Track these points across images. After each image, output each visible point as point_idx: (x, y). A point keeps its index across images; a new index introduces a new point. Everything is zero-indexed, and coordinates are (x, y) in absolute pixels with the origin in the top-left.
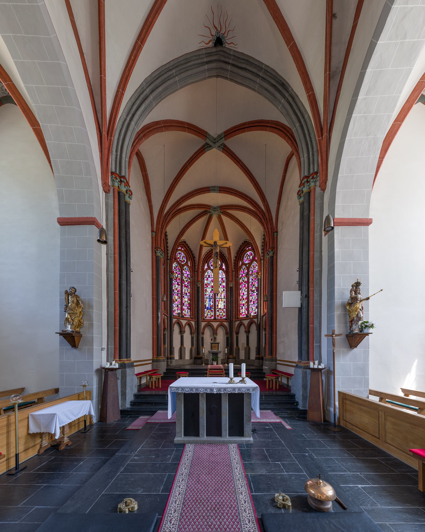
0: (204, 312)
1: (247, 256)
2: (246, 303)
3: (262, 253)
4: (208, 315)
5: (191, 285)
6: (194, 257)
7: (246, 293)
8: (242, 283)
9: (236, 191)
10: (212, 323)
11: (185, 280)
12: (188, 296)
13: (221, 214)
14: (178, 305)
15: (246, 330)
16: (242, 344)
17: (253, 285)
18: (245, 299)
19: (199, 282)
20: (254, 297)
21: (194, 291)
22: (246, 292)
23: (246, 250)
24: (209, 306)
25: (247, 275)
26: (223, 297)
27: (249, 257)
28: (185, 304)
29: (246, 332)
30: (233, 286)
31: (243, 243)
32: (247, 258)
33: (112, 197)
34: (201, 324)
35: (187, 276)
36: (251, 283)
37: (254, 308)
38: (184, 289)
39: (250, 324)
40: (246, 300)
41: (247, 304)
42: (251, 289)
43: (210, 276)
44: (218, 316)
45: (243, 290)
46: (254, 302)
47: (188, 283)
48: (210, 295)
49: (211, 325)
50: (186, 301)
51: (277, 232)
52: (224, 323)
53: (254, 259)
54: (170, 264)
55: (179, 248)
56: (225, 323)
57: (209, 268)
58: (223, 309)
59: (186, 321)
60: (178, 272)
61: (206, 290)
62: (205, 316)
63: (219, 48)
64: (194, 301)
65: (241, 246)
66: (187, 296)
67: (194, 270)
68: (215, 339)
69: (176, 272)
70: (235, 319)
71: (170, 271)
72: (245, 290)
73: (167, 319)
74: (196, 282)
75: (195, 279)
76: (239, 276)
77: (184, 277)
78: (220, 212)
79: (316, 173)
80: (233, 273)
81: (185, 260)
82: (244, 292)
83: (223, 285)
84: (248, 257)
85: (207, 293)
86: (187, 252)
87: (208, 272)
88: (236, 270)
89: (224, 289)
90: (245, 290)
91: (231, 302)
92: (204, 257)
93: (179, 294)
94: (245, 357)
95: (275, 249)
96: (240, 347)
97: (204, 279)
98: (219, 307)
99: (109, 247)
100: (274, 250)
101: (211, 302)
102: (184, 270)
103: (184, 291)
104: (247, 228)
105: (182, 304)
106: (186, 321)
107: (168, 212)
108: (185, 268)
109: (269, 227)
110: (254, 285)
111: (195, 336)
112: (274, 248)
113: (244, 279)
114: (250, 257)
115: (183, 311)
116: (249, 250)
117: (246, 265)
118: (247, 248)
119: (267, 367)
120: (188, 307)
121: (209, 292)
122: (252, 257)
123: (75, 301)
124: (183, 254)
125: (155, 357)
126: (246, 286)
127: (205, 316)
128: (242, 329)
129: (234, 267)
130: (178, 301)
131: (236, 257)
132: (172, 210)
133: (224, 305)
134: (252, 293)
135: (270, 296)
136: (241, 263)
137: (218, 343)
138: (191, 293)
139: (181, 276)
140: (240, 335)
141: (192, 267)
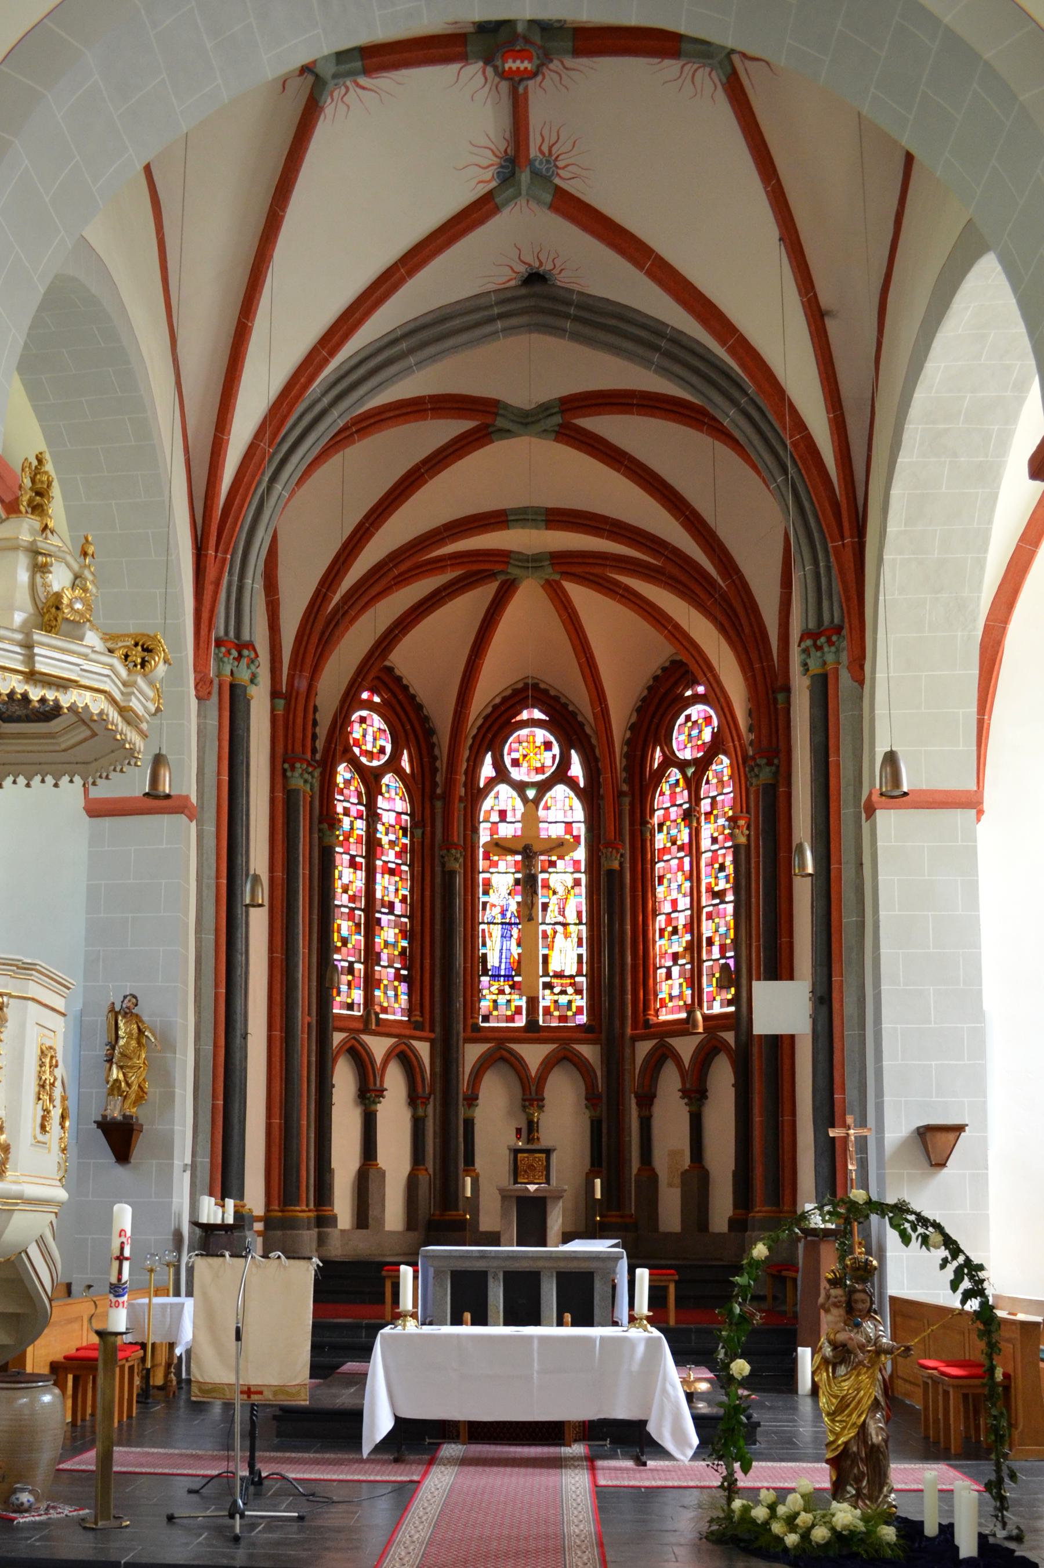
0: (475, 992)
1: (690, 724)
2: (686, 949)
4: (496, 1007)
6: (430, 732)
7: (688, 899)
8: (665, 850)
9: (633, 460)
10: (516, 1047)
11: (385, 840)
13: (557, 577)
15: (688, 1086)
16: (673, 1154)
17: (716, 866)
18: (680, 932)
19: (453, 851)
21: (428, 893)
24: (501, 962)
25: (689, 816)
26: (571, 917)
27: (695, 733)
28: (384, 956)
29: (685, 1093)
30: (621, 864)
32: (689, 735)
33: (216, 708)
34: (461, 1051)
36: (710, 854)
40: (688, 937)
41: (692, 958)
42: (709, 889)
43: (509, 814)
44: (547, 1011)
45: (674, 886)
46: (723, 948)
47: (398, 855)
48: (508, 905)
49: (513, 1059)
50: (391, 940)
52: (577, 1047)
56: (588, 1051)
58: (572, 977)
59: (389, 1042)
60: (353, 812)
61: (487, 884)
62: (483, 1011)
63: (537, 289)
64: (427, 939)
65: (656, 678)
67: (427, 790)
68: (531, 1129)
69: (345, 808)
70: (634, 1027)
72: (680, 886)
74: (441, 849)
76: (652, 815)
77: (380, 827)
79: (838, 630)
80: (620, 804)
81: (388, 748)
82: (674, 895)
84: (691, 729)
85: (493, 898)
86: (398, 708)
87: (497, 797)
88: (637, 787)
89: (577, 876)
90: (680, 886)
91: (616, 942)
92: (479, 728)
93: (360, 909)
94: (683, 1222)
98: (554, 966)
99: (205, 856)
100: (776, 761)
101: (514, 942)
102: (382, 794)
103: (379, 895)
104: (677, 627)
105: (371, 956)
106: (389, 1042)
108: (388, 786)
110: (722, 868)
111: (431, 1112)
112: (776, 753)
113: (674, 832)
114: (700, 732)
115: (377, 993)
116: (697, 699)
117: (682, 765)
120: (398, 970)
121: (504, 891)
123: (135, 1031)
124: (377, 721)
126: (687, 867)
127: (483, 1011)
128: (670, 1082)
129: (624, 775)
130: (354, 947)
131: (633, 728)
132: (350, 603)
133: (580, 956)
134: (714, 905)
135: (765, 949)
136: (658, 753)
137: (548, 1152)
139: (368, 826)
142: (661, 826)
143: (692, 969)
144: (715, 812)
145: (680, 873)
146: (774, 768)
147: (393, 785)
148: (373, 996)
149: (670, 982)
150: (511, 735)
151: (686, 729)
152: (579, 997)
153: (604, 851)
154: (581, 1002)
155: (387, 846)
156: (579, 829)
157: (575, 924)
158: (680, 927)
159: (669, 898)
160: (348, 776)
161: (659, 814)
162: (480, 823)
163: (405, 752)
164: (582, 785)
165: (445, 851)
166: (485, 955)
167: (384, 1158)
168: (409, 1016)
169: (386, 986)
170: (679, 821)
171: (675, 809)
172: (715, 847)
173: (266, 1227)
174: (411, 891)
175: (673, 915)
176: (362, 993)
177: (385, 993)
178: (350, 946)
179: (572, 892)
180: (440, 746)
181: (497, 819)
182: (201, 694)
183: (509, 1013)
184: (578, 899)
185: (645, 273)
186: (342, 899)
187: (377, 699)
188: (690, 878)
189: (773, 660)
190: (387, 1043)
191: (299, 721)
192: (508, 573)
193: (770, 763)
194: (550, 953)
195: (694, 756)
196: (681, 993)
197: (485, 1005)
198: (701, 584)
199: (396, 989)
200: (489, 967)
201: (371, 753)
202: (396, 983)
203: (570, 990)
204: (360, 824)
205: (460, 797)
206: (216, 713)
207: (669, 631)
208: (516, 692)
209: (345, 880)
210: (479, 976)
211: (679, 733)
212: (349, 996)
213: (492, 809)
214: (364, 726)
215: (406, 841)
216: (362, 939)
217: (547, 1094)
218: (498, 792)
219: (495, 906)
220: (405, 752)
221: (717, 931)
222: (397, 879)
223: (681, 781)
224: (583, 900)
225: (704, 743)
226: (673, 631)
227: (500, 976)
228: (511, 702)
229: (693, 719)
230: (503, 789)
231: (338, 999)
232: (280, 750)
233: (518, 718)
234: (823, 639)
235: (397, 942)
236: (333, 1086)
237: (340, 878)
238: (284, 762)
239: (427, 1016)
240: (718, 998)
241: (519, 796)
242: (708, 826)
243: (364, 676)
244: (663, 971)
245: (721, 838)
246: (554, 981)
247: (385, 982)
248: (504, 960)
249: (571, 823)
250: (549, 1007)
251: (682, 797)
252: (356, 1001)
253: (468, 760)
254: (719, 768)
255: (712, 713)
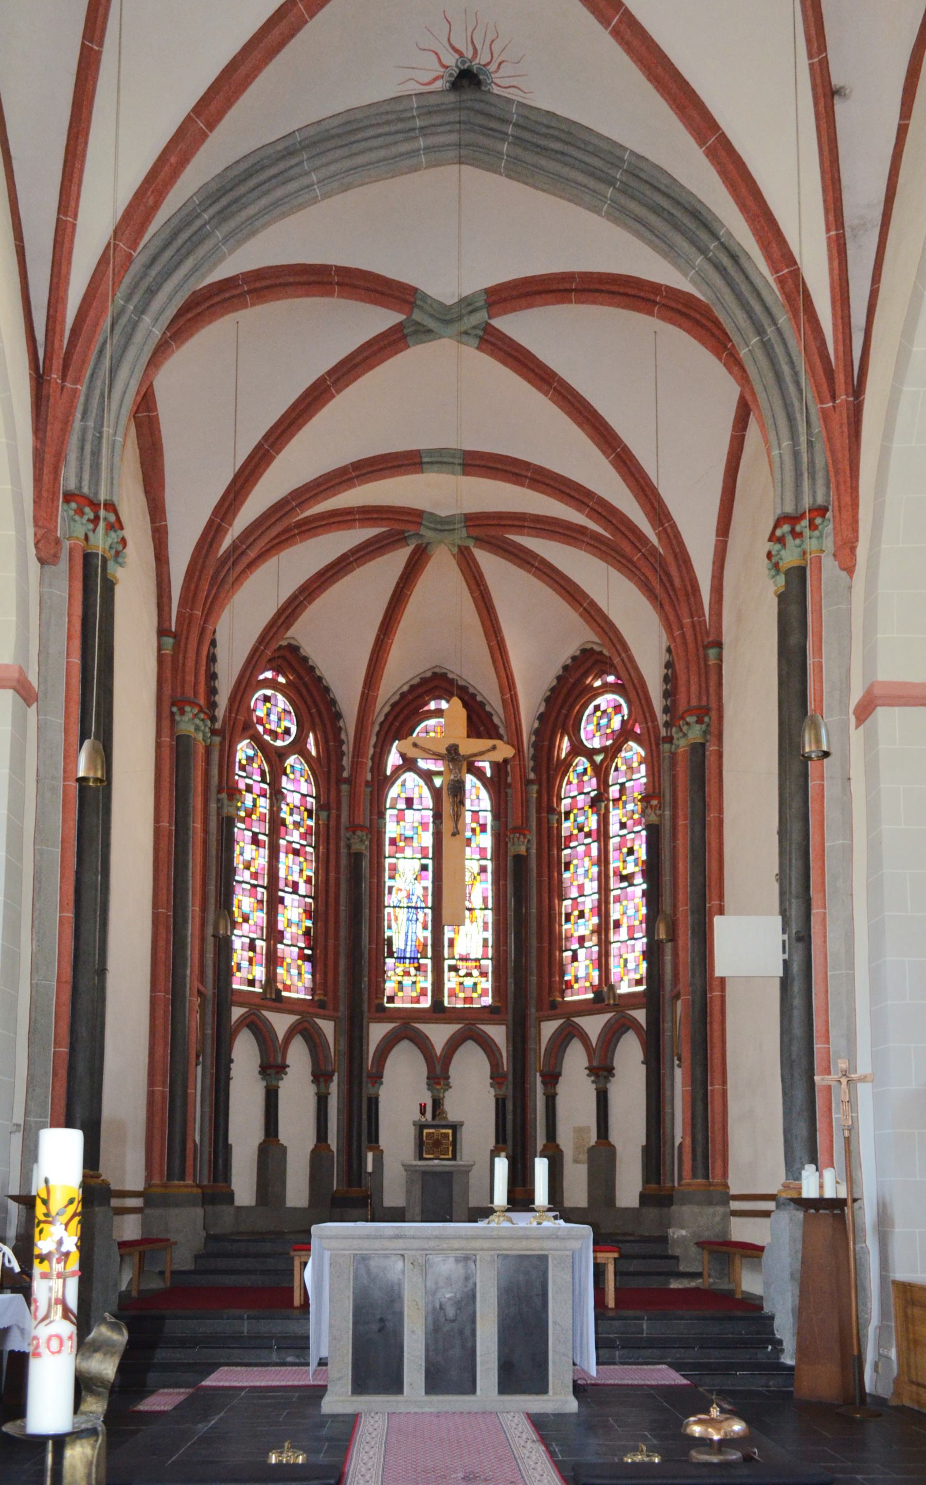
1: (599, 714)
2: (593, 932)
3: (666, 710)
5: (317, 841)
7: (595, 884)
8: (570, 838)
11: (289, 820)
12: (304, 897)
13: (471, 544)
14: (252, 941)
15: (595, 1064)
16: (580, 1131)
17: (625, 850)
19: (359, 833)
20: (631, 905)
22: (592, 880)
23: (590, 686)
24: (406, 945)
25: (599, 802)
27: (604, 722)
28: (287, 935)
29: (593, 1071)
30: (528, 850)
31: (574, 658)
32: (598, 724)
35: (297, 803)
36: (618, 839)
37: (631, 957)
38: (286, 861)
39: (611, 1036)
42: (617, 873)
43: (415, 801)
44: (452, 993)
45: (581, 871)
46: (631, 929)
47: (303, 836)
50: (295, 919)
51: (719, 645)
53: (624, 735)
54: (221, 752)
55: (261, 677)
57: (409, 764)
58: (477, 960)
60: (256, 789)
61: (394, 868)
63: (469, 96)
65: (566, 668)
66: (300, 896)
67: (333, 773)
71: (220, 782)
72: (587, 871)
73: (202, 1006)
75: (339, 817)
77: (284, 806)
78: (469, 537)
79: (822, 511)
82: (581, 880)
83: (478, 846)
84: (600, 718)
85: (397, 883)
86: (304, 692)
87: (403, 785)
88: (544, 777)
89: (483, 862)
90: (587, 871)
91: (521, 922)
92: (387, 716)
94: (590, 1196)
95: (714, 714)
96: (562, 1147)
97: (382, 815)
98: (459, 950)
100: (706, 719)
101: (420, 925)
103: (282, 874)
104: (593, 603)
105: (274, 934)
107: (234, 546)
108: (292, 767)
109: (687, 621)
110: (631, 852)
112: (706, 710)
114: (610, 720)
115: (280, 970)
116: (607, 688)
117: (590, 754)
118: (595, 678)
119: (684, 1232)
120: (301, 949)
122: (623, 721)
124: (282, 702)
125: (158, 1182)
126: (594, 852)
127: (388, 992)
130: (256, 925)
131: (542, 718)
136: (566, 744)
138: (316, 880)
139: (272, 805)
140: (563, 1089)
141: (324, 762)
142: (567, 814)
143: (600, 952)
144: (624, 798)
145: (587, 859)
146: (704, 726)
147: (298, 767)
148: (275, 974)
149: (575, 964)
150: (418, 725)
151: (595, 719)
152: (484, 979)
153: (512, 836)
154: (486, 984)
155: (291, 827)
156: (485, 817)
157: (481, 909)
158: (587, 912)
159: (575, 883)
160: (251, 753)
161: (566, 802)
162: (386, 809)
163: (311, 735)
164: (489, 774)
165: (351, 833)
166: (390, 939)
167: (285, 1135)
168: (312, 995)
169: (289, 965)
170: (586, 808)
171: (582, 796)
172: (624, 832)
173: (147, 1204)
174: (316, 872)
175: (580, 900)
176: (264, 969)
177: (288, 971)
178: (251, 922)
179: (478, 878)
180: (346, 730)
181: (404, 806)
182: (43, 554)
183: (414, 994)
184: (484, 885)
185: (611, 33)
186: (243, 875)
187: (281, 680)
188: (598, 863)
189: (704, 615)
190: (290, 1019)
191: (190, 663)
192: (422, 536)
193: (700, 721)
194: (456, 936)
195: (603, 745)
196: (588, 975)
197: (390, 987)
198: (626, 536)
199: (299, 967)
200: (394, 949)
201: (276, 733)
202: (300, 962)
203: (475, 973)
204: (263, 803)
205: (367, 782)
206: (66, 583)
207: (584, 609)
208: (424, 681)
209: (247, 856)
210: (385, 958)
211: (588, 723)
212: (250, 972)
213: (399, 796)
214: (268, 705)
215: (311, 823)
216: (265, 916)
217: (452, 1071)
218: (405, 781)
219: (401, 890)
220: (311, 735)
221: (624, 913)
222: (301, 859)
223: (589, 770)
224: (489, 885)
225: (613, 732)
226: (589, 609)
227: (405, 958)
228: (420, 691)
229: (602, 708)
230: (410, 778)
231: (238, 974)
232: (167, 690)
233: (426, 708)
234: (805, 522)
235: (301, 921)
236: (232, 1061)
237: (241, 854)
238: (173, 704)
239: (330, 994)
240: (626, 978)
241: (426, 784)
242: (617, 812)
243: (268, 643)
244: (569, 953)
245: (630, 823)
246: (460, 964)
247: (288, 960)
248: (409, 943)
249: (477, 812)
250: (454, 989)
251: (591, 784)
252: (257, 978)
253: (375, 746)
254: (628, 755)
255: (622, 701)
